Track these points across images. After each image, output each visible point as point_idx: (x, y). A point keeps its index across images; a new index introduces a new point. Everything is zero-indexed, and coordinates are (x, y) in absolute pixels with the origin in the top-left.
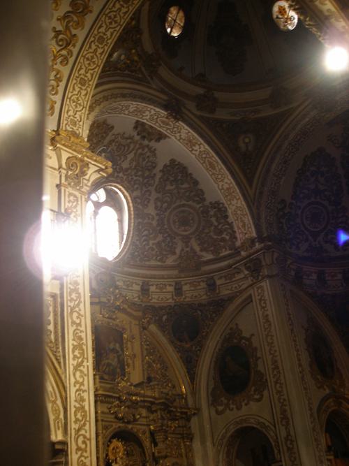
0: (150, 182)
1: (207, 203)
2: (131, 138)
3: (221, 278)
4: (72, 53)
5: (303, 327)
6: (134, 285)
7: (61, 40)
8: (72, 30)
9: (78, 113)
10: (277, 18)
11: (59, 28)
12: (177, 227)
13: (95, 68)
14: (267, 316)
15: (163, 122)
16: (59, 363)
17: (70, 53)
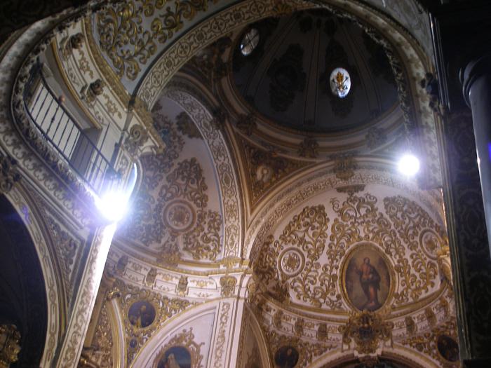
0: (165, 169)
1: (206, 210)
2: (170, 124)
3: (194, 281)
4: (172, 35)
5: (248, 353)
6: (114, 255)
7: (169, 21)
8: (182, 16)
9: (154, 88)
10: (333, 81)
11: (173, 10)
12: (182, 224)
13: (184, 57)
14: (224, 331)
15: (205, 124)
16: (68, 302)
17: (171, 35)
